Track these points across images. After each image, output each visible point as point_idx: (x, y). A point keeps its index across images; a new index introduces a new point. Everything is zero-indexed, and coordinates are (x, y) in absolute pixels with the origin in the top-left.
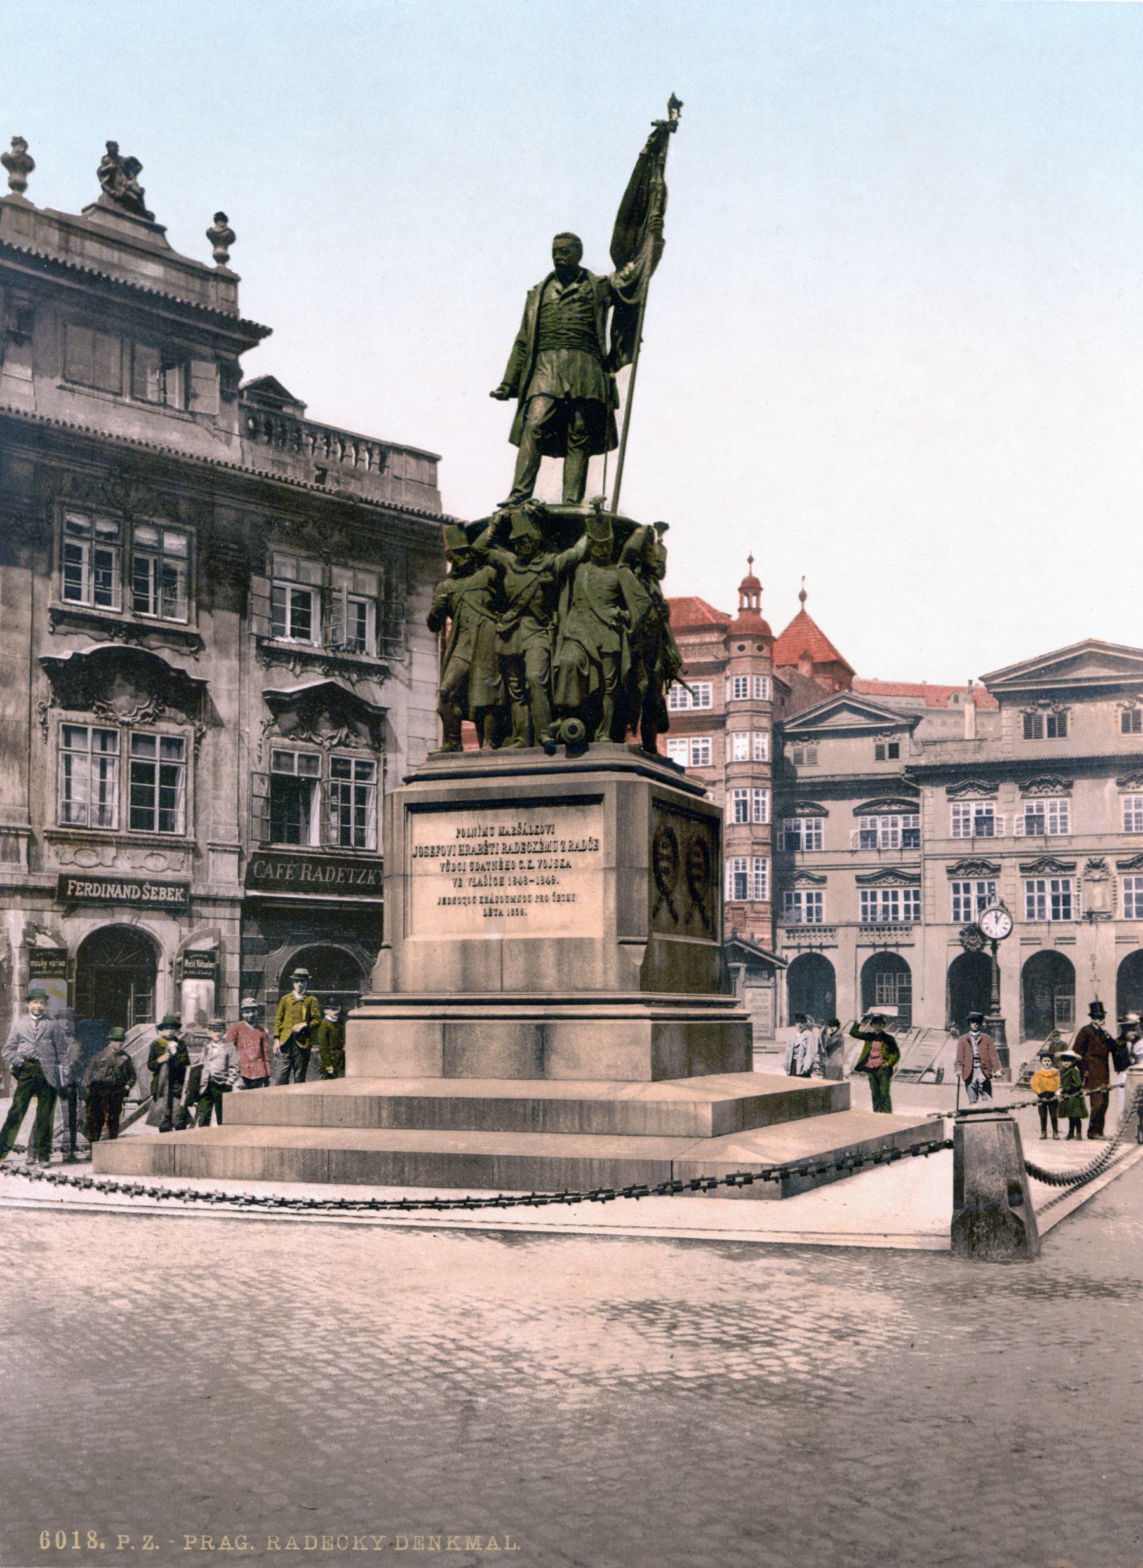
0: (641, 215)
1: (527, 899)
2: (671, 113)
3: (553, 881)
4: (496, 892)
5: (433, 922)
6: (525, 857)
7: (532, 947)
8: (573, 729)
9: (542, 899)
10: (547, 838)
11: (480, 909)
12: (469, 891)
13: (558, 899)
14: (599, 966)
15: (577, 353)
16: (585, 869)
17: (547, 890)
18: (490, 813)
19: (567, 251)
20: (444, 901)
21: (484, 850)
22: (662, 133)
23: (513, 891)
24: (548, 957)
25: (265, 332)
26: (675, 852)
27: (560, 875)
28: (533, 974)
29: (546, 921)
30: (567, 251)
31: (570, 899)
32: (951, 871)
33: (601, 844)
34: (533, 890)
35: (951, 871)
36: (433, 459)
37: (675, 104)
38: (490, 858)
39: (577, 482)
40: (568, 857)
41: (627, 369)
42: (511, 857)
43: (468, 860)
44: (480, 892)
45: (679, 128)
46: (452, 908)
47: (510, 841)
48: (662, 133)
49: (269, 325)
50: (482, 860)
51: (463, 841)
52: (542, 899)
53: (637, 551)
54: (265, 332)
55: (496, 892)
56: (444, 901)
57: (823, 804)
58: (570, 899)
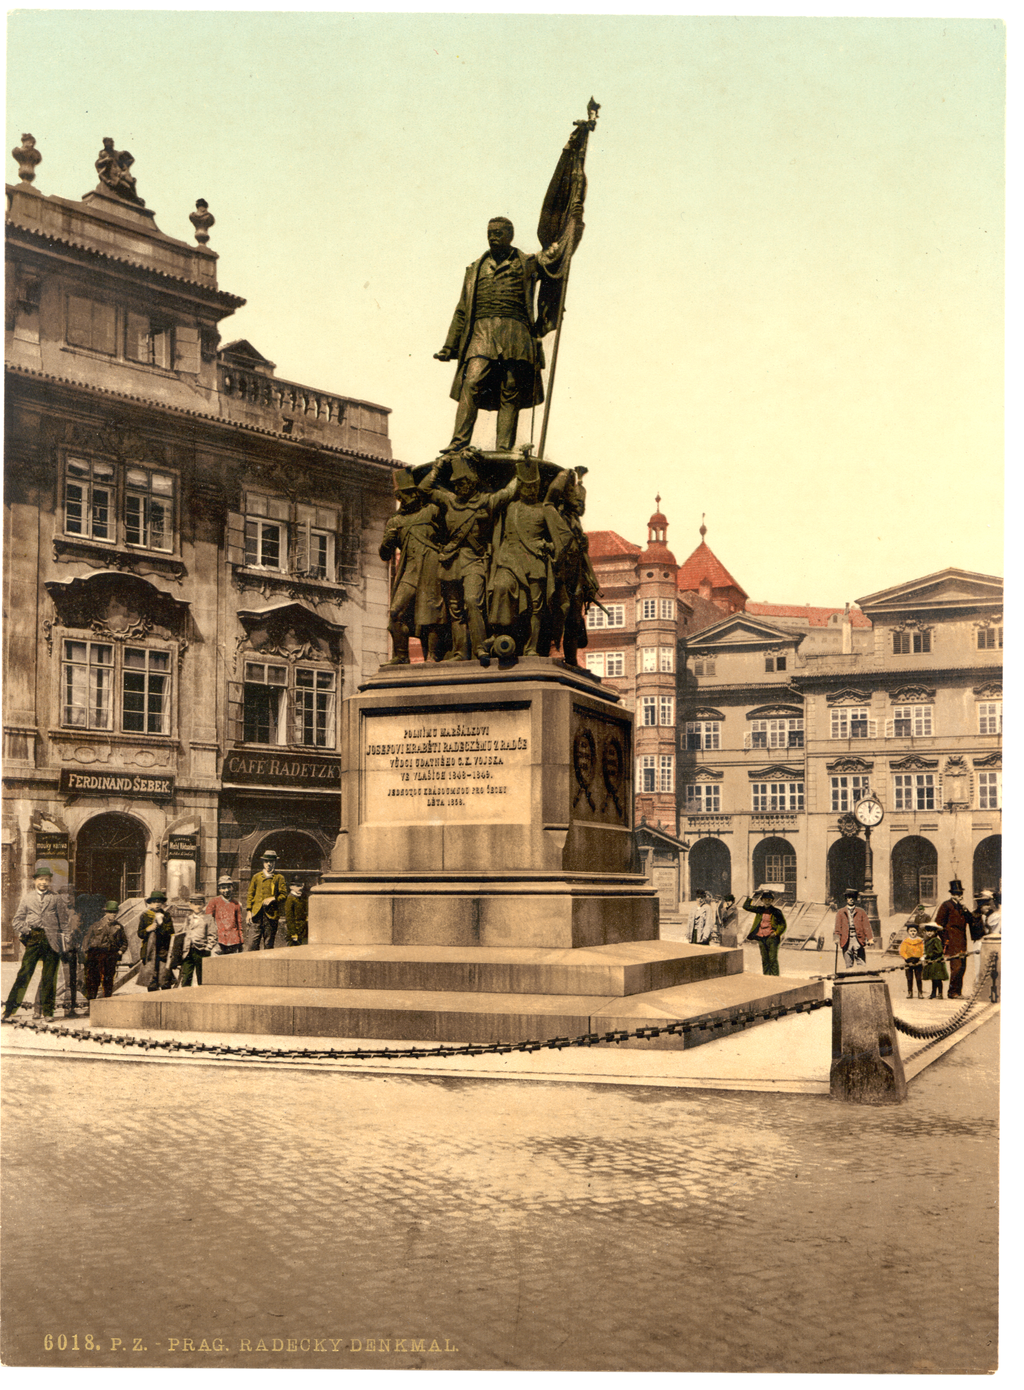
1: (465, 791)
2: (590, 114)
3: (487, 776)
4: (439, 784)
5: (384, 811)
6: (464, 755)
7: (469, 832)
9: (478, 791)
10: (482, 738)
11: (425, 799)
12: (415, 784)
13: (492, 791)
14: (527, 848)
15: (509, 321)
16: (515, 765)
17: (482, 784)
18: (433, 717)
19: (501, 233)
20: (394, 793)
22: (582, 131)
23: (452, 784)
24: (483, 842)
25: (241, 302)
27: (494, 770)
28: (470, 855)
29: (481, 810)
30: (501, 233)
31: (502, 791)
32: (830, 768)
34: (470, 783)
35: (830, 768)
36: (385, 412)
37: (593, 106)
38: (433, 756)
39: (508, 432)
41: (552, 334)
43: (414, 757)
46: (400, 798)
47: (451, 741)
48: (582, 131)
49: (243, 296)
50: (426, 757)
51: (410, 741)
52: (478, 791)
53: (560, 491)
54: (241, 302)
55: (439, 784)
58: (502, 791)
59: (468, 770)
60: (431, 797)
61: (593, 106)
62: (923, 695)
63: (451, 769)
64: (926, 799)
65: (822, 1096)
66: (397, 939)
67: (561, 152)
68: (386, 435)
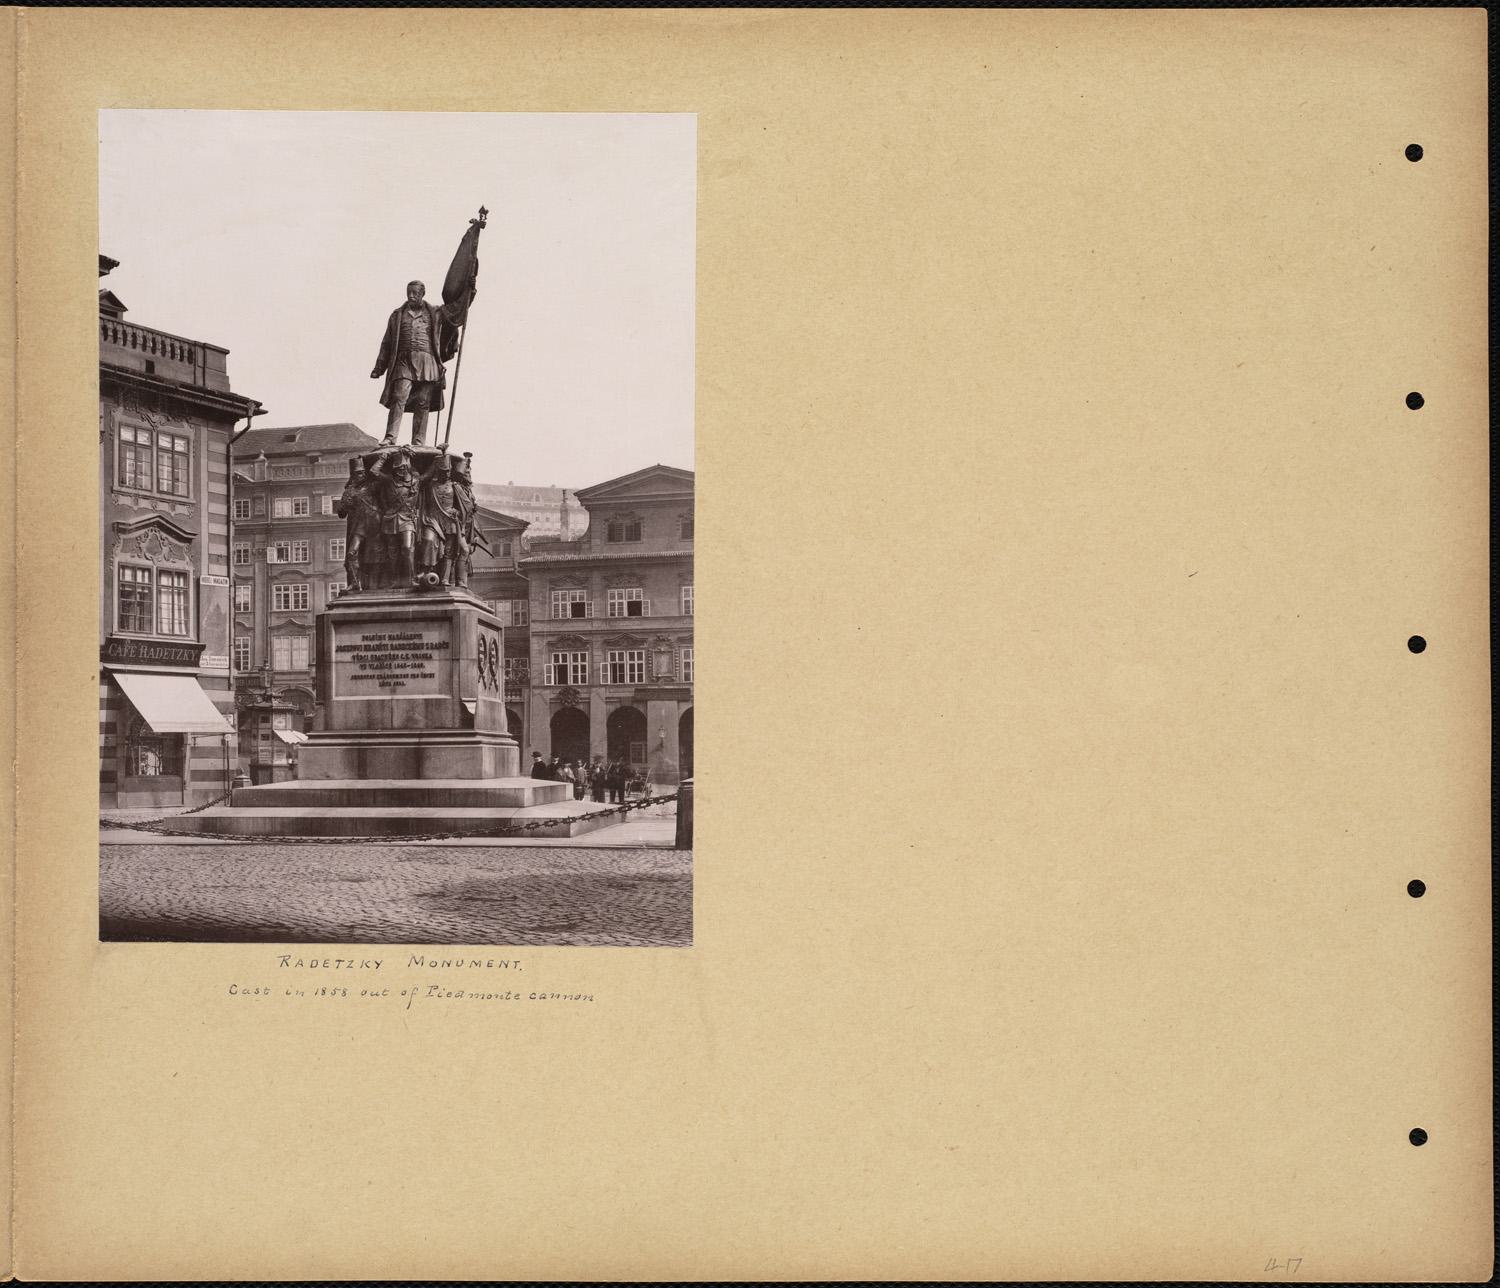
0: (462, 284)
1: (406, 676)
2: (481, 217)
3: (421, 666)
4: (387, 672)
6: (404, 653)
8: (433, 579)
10: (417, 641)
11: (377, 682)
12: (369, 672)
13: (425, 676)
14: (450, 714)
15: (419, 348)
17: (416, 671)
19: (415, 289)
20: (355, 678)
21: (379, 648)
22: (477, 226)
25: (101, 257)
26: (490, 659)
27: (426, 663)
30: (415, 289)
33: (437, 675)
34: (409, 671)
36: (226, 352)
37: (483, 211)
39: (418, 429)
40: (429, 652)
41: (454, 361)
42: (396, 652)
43: (369, 654)
44: (377, 672)
45: (486, 226)
46: (359, 682)
47: (395, 643)
48: (477, 226)
49: (117, 260)
50: (378, 653)
51: (366, 643)
53: (455, 470)
55: (387, 672)
56: (355, 678)
57: (383, 378)
59: (409, 663)
60: (381, 681)
61: (483, 211)
62: (635, 579)
63: (396, 662)
64: (636, 673)
65: (670, 849)
66: (362, 776)
67: (654, 464)
68: (225, 373)
